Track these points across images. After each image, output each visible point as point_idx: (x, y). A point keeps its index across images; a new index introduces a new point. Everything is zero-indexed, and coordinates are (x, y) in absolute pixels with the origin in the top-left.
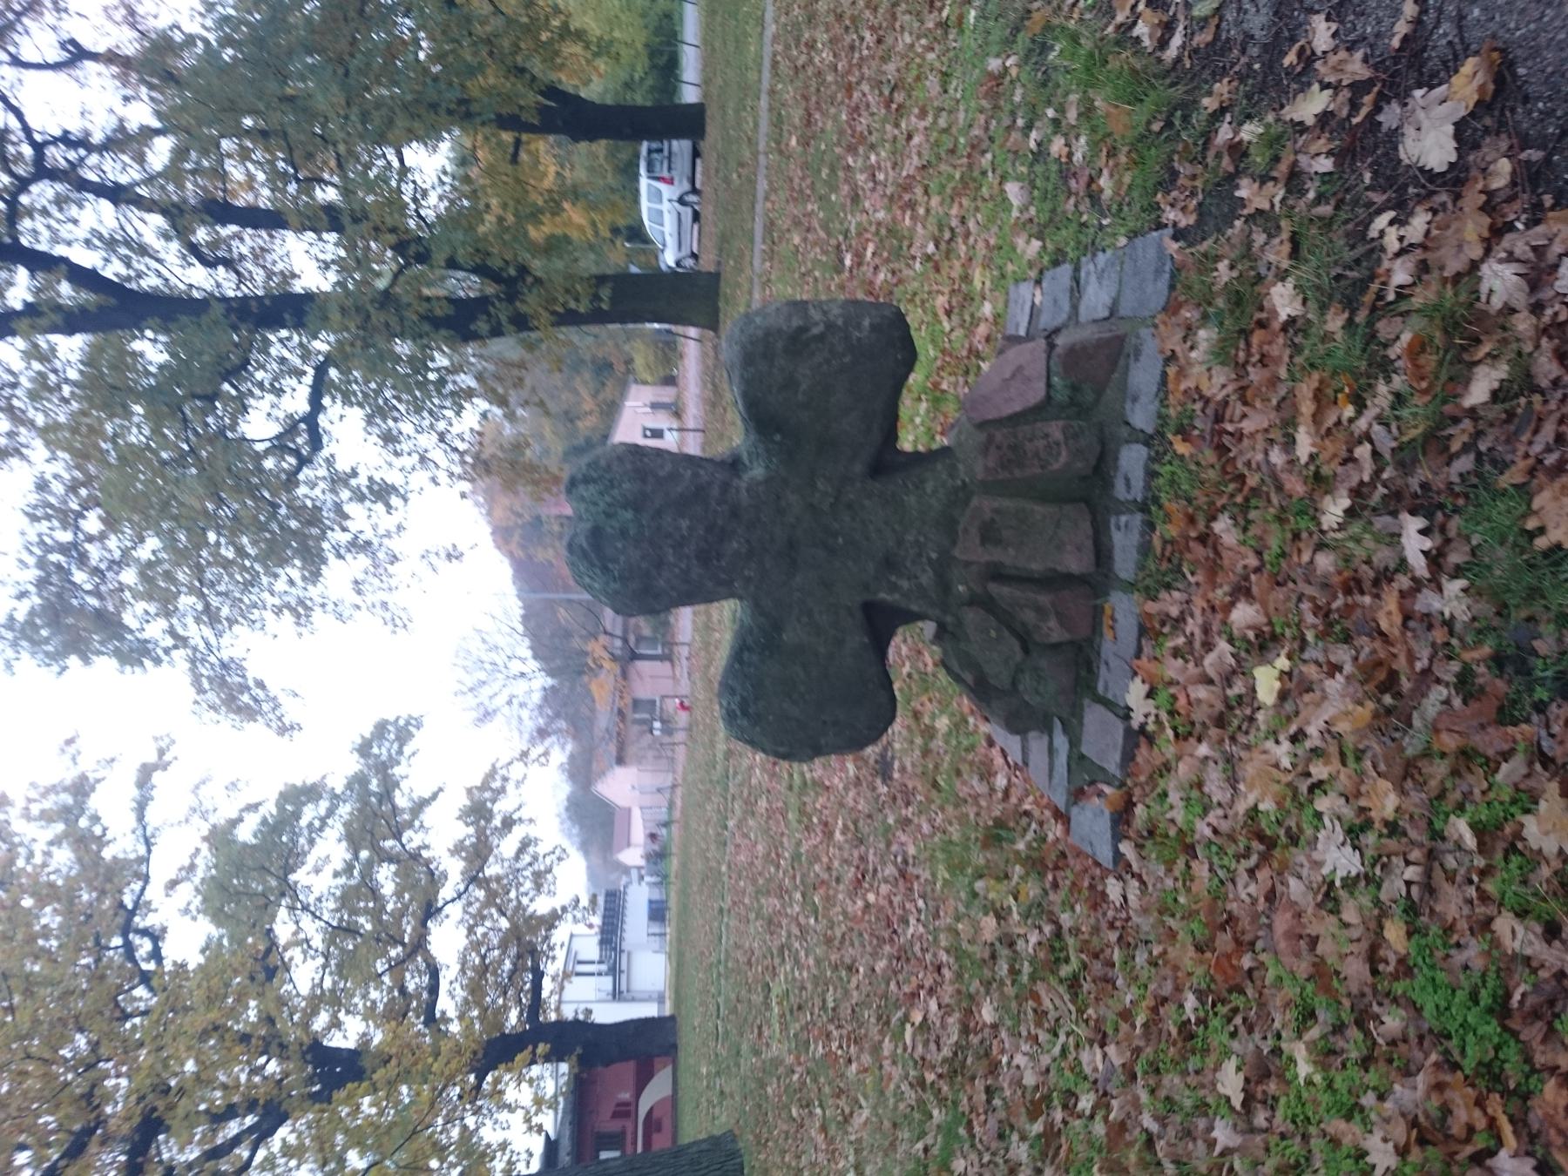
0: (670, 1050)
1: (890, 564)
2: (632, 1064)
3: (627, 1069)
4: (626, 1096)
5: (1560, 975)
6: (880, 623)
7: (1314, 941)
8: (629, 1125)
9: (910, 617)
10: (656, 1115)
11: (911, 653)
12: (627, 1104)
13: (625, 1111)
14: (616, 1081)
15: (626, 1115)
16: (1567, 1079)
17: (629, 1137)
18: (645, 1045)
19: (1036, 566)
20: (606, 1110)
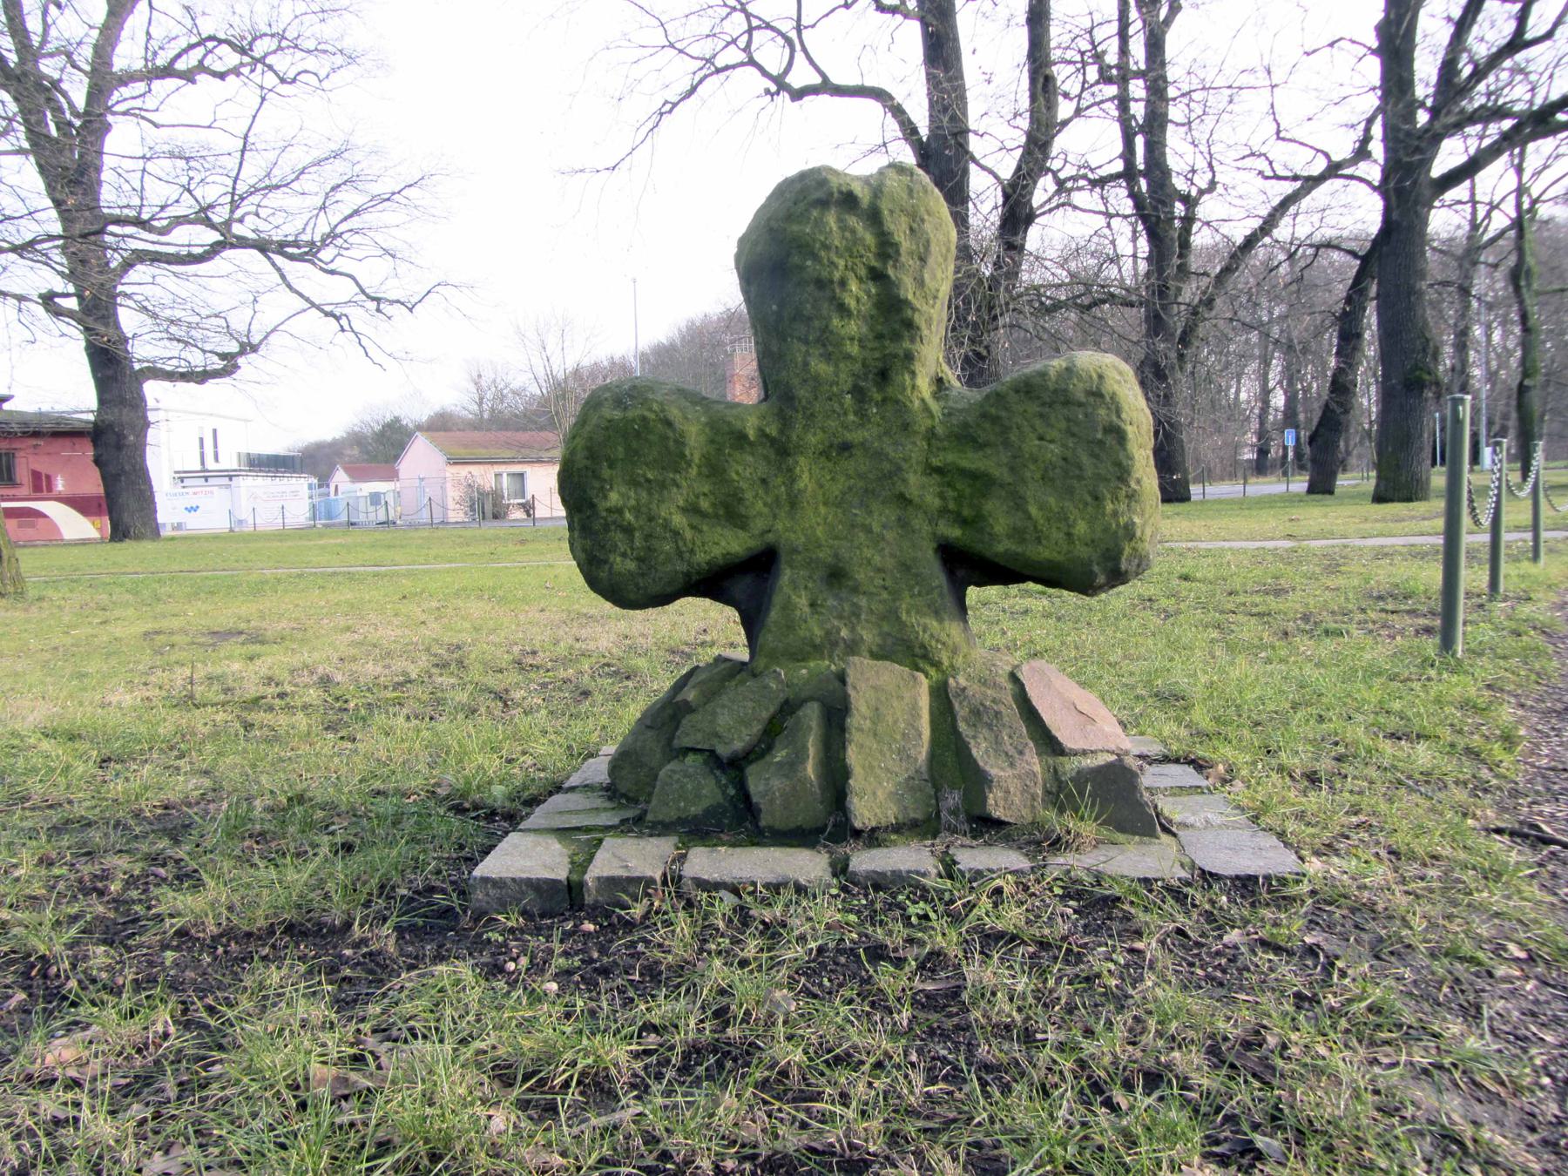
0: (119, 533)
1: (836, 576)
2: (99, 490)
3: (93, 485)
4: (60, 485)
5: (1006, 1172)
6: (743, 581)
7: (869, 562)
8: (25, 491)
9: (752, 623)
10: (41, 520)
11: (708, 627)
12: (50, 489)
13: (41, 485)
14: (78, 472)
15: (37, 488)
16: (754, 1173)
17: (11, 492)
18: (122, 500)
19: (853, 756)
20: (42, 466)
